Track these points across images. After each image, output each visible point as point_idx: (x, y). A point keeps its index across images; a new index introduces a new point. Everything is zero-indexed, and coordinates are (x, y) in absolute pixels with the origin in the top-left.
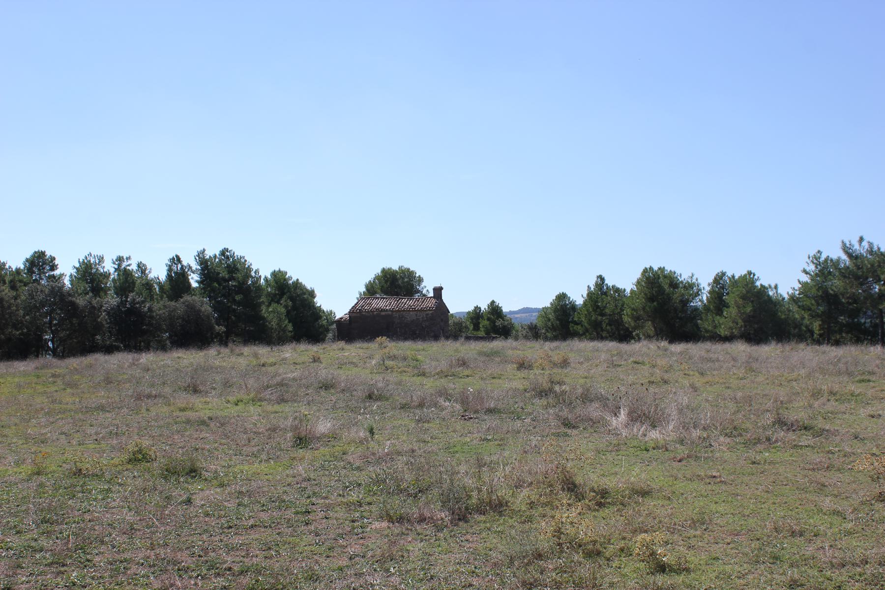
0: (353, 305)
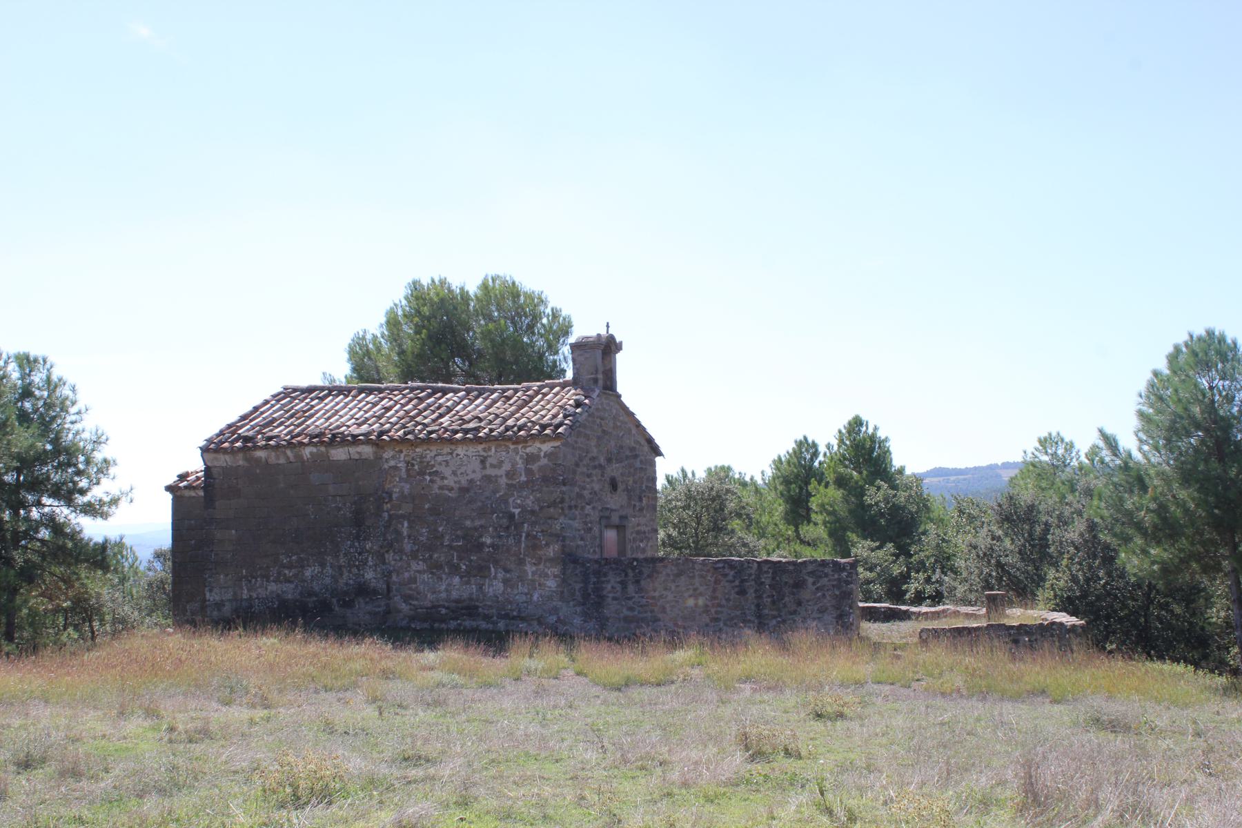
0: (233, 418)
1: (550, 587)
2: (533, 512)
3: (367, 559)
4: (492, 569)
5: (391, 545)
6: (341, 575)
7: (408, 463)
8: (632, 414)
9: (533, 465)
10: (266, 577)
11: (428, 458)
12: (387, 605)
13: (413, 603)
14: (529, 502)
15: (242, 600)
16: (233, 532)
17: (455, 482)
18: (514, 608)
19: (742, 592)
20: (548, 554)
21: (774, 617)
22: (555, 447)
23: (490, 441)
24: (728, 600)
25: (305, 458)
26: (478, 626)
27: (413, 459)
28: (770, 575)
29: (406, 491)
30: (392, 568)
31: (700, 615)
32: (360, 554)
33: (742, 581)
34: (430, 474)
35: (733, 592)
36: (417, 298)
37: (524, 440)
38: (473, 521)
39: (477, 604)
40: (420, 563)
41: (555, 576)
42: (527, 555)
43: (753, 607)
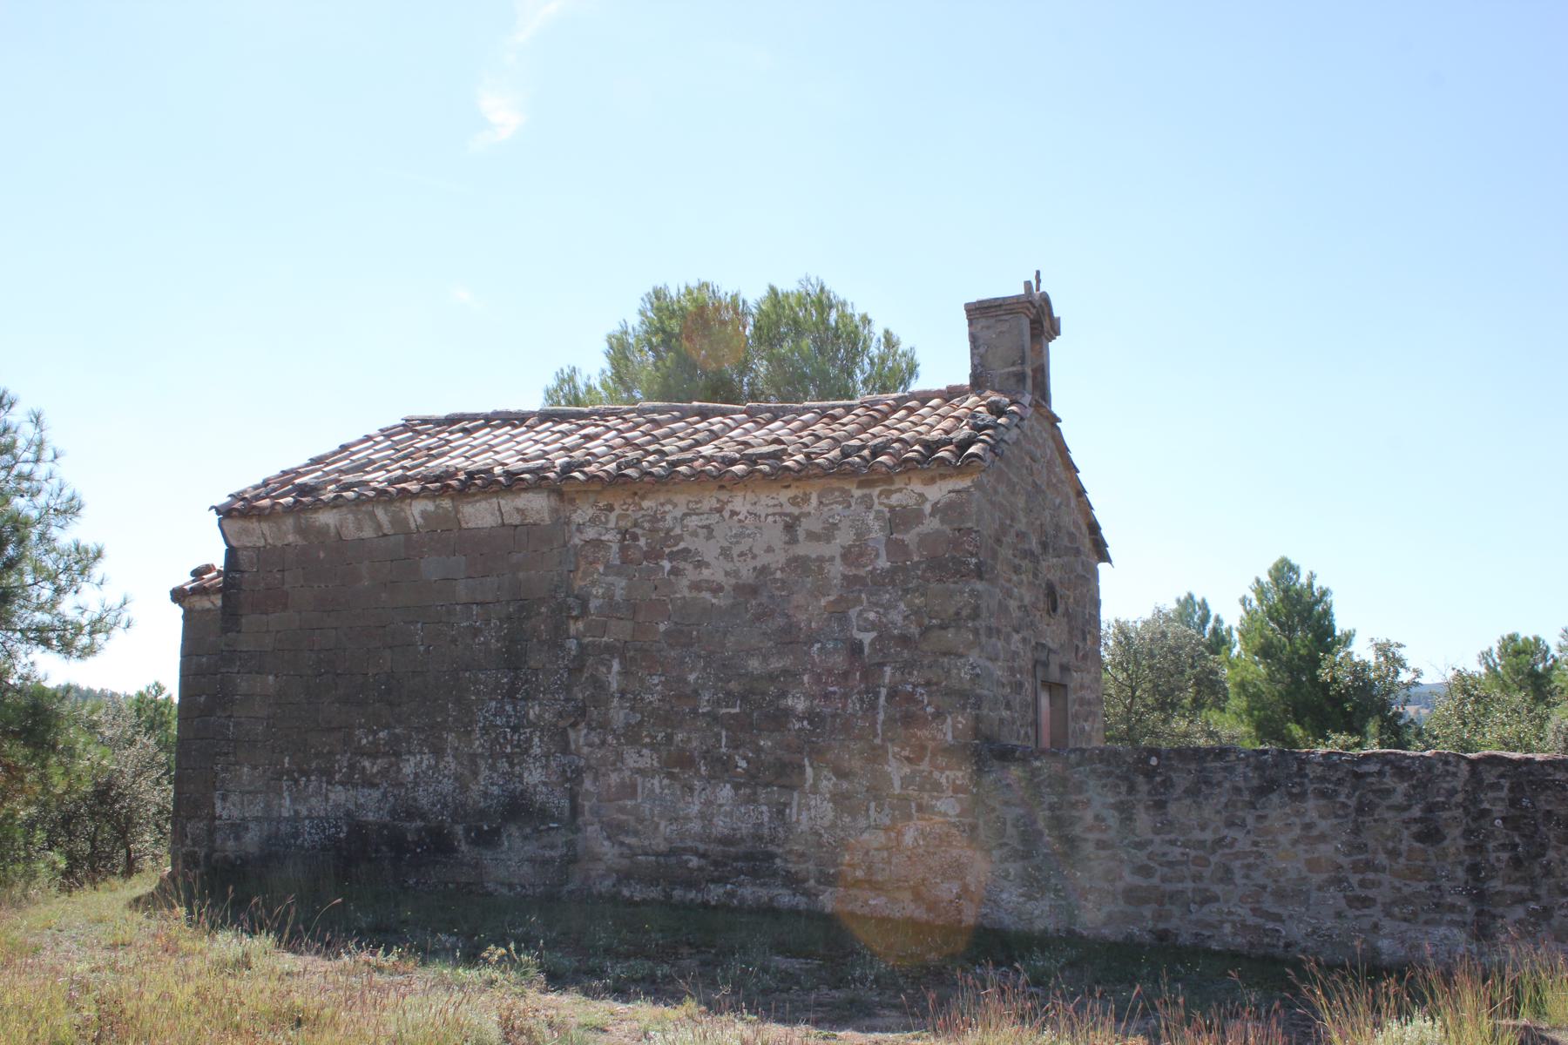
1: (945, 815)
2: (905, 640)
3: (529, 740)
4: (809, 771)
5: (582, 712)
6: (475, 774)
7: (624, 533)
8: (1072, 468)
9: (907, 531)
10: (327, 774)
11: (669, 522)
12: (570, 844)
13: (627, 840)
14: (896, 616)
15: (280, 819)
16: (271, 678)
17: (727, 574)
18: (856, 860)
19: (1430, 835)
20: (940, 736)
21: (1520, 900)
22: (958, 492)
23: (809, 477)
24: (1394, 854)
25: (413, 526)
26: (771, 899)
27: (636, 525)
28: (1504, 794)
29: (619, 595)
30: (582, 763)
31: (1320, 888)
32: (515, 729)
33: (1431, 808)
34: (672, 557)
35: (1406, 833)
36: (659, 310)
37: (888, 476)
38: (765, 659)
39: (771, 848)
40: (644, 751)
41: (957, 790)
42: (892, 740)
43: (1460, 873)
